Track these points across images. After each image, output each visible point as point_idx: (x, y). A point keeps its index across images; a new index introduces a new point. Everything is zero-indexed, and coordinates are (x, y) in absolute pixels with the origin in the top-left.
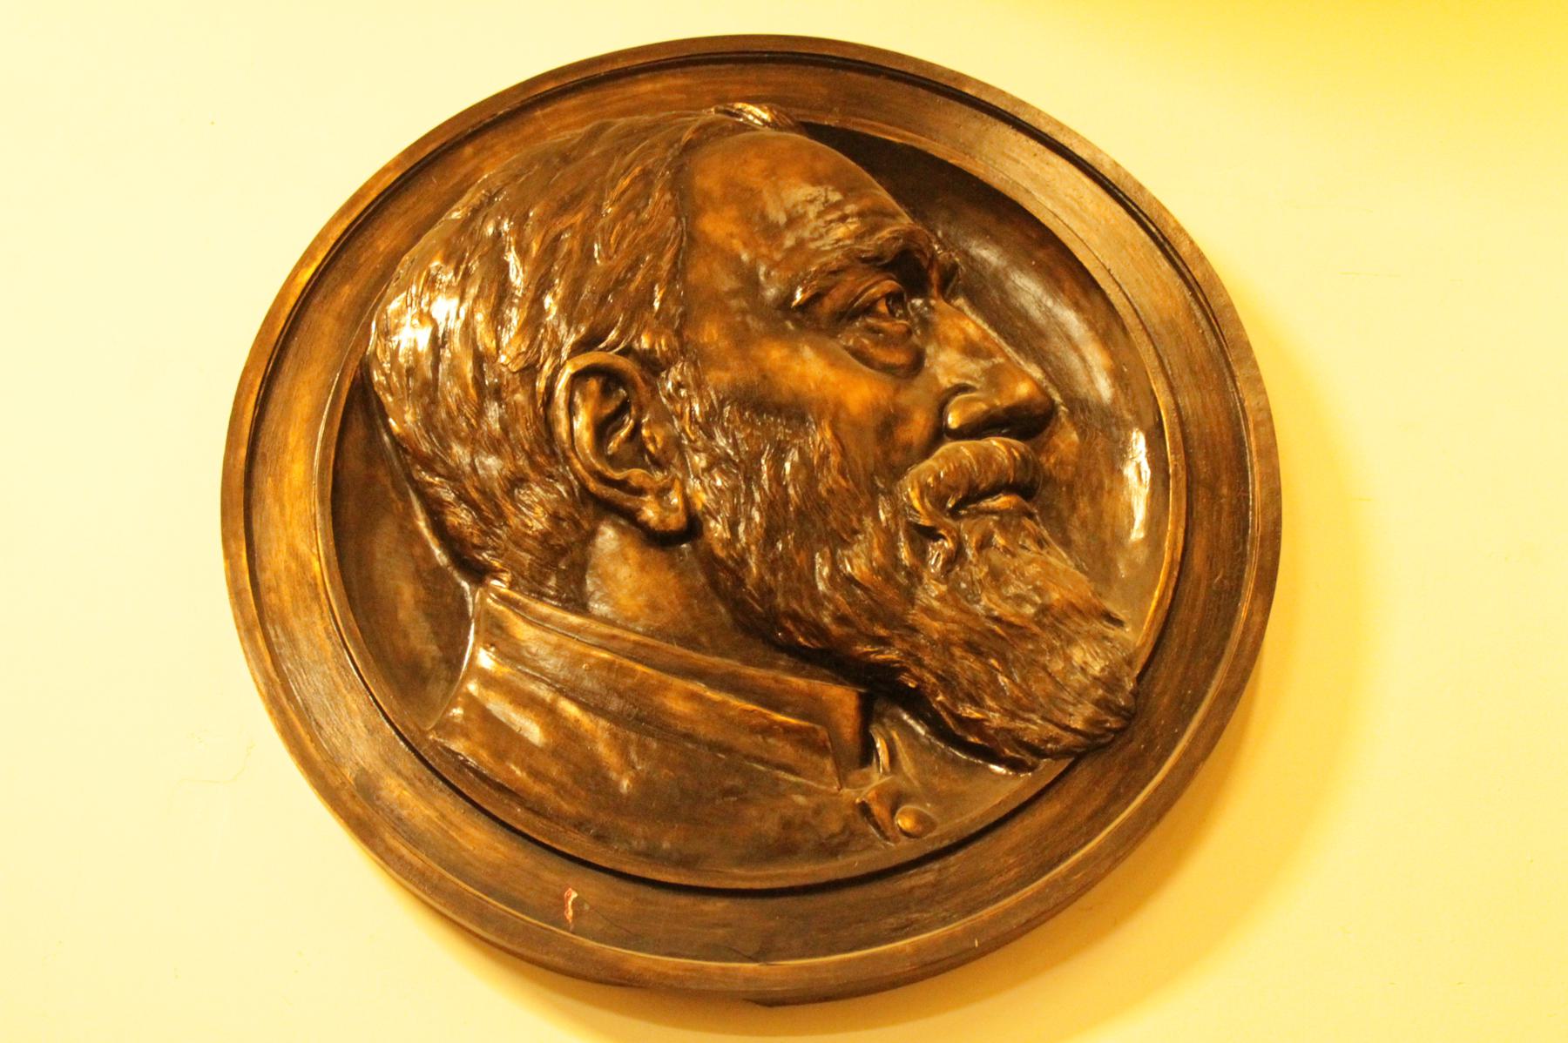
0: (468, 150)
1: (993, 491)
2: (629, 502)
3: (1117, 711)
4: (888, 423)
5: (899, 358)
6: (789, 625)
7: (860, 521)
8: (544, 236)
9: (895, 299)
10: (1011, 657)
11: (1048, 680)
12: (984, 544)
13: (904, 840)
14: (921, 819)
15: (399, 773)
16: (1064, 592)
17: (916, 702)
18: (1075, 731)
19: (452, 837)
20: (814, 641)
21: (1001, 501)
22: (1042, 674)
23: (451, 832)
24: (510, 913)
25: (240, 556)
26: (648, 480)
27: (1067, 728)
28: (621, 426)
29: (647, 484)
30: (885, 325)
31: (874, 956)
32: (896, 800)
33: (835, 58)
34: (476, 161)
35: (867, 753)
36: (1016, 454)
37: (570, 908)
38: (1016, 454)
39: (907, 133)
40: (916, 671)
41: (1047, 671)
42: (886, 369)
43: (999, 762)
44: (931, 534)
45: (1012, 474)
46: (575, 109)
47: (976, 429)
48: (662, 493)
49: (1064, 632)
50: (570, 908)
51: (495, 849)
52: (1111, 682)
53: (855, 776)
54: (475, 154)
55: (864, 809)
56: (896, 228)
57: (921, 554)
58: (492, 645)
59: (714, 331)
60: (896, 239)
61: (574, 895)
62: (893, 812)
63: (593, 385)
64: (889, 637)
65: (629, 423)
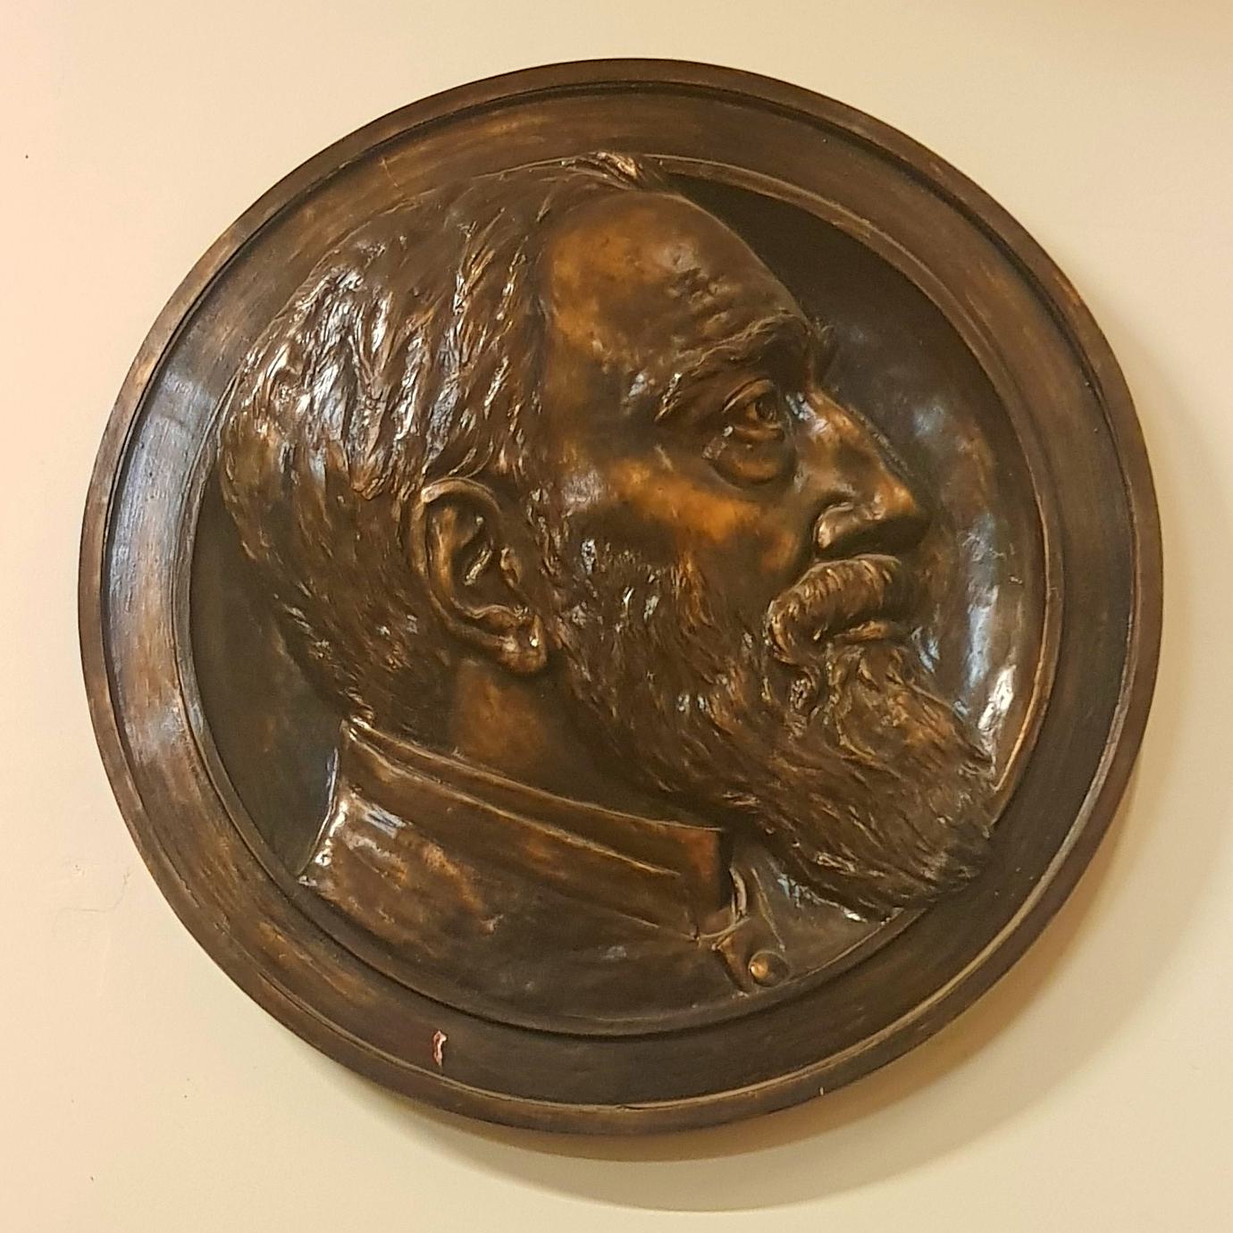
0: (309, 212)
1: (862, 618)
2: (490, 641)
3: (972, 860)
4: (753, 542)
5: (768, 468)
6: (649, 770)
7: (722, 659)
8: (393, 340)
9: (767, 403)
10: (869, 802)
11: (905, 827)
12: (852, 674)
13: (758, 991)
14: (776, 966)
15: (273, 918)
16: (929, 730)
17: (775, 845)
18: (929, 881)
19: (326, 981)
20: (674, 786)
21: (874, 628)
22: (901, 821)
23: (325, 977)
24: (384, 1058)
25: (104, 694)
26: (507, 618)
27: (922, 878)
28: (477, 558)
29: (507, 620)
30: (754, 433)
31: (719, 1102)
32: (751, 945)
33: (713, 88)
34: (318, 225)
35: (729, 892)
36: (888, 577)
37: (439, 1051)
38: (888, 577)
39: (789, 186)
40: (774, 817)
41: (905, 819)
42: (757, 482)
43: (854, 910)
44: (795, 672)
45: (881, 598)
46: (425, 157)
47: (845, 548)
48: (523, 631)
49: (925, 776)
50: (439, 1051)
51: (367, 993)
52: (966, 829)
53: (713, 920)
54: (316, 218)
55: (719, 955)
56: (770, 320)
57: (783, 692)
58: (358, 786)
59: (574, 451)
60: (769, 334)
61: (443, 1039)
62: (746, 963)
63: (449, 514)
64: (748, 784)
65: (486, 556)
